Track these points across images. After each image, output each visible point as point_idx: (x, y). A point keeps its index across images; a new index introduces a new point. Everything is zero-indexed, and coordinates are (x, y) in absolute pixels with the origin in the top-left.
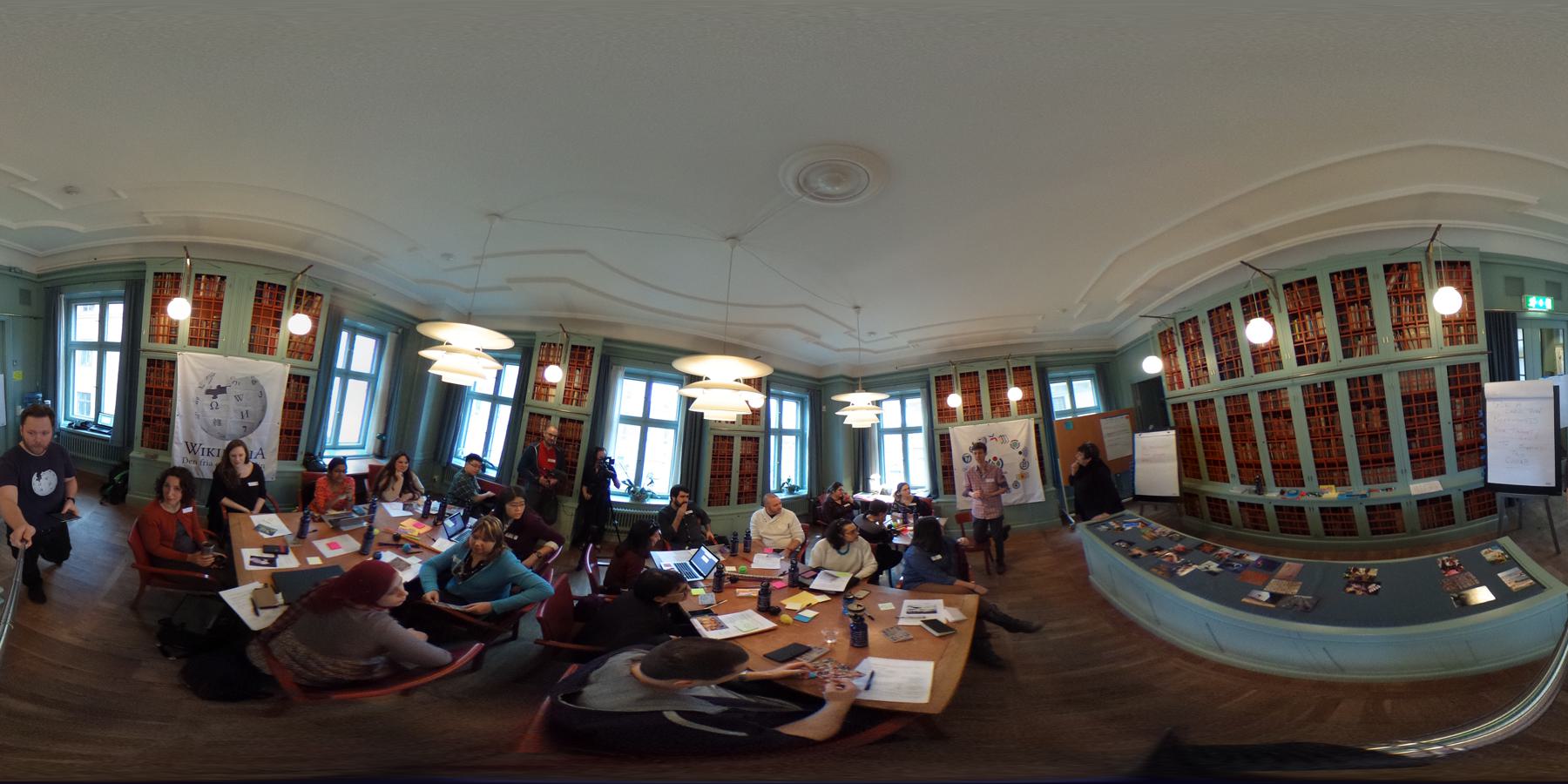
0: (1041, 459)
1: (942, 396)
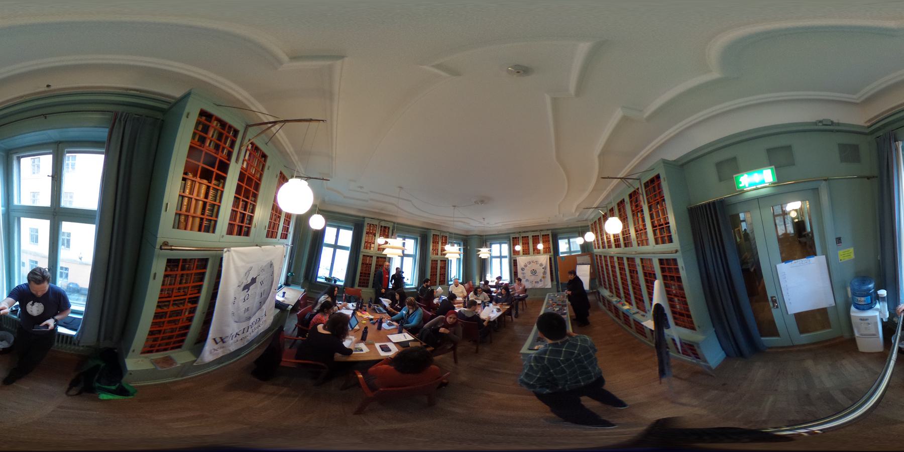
0: (551, 271)
1: (514, 245)
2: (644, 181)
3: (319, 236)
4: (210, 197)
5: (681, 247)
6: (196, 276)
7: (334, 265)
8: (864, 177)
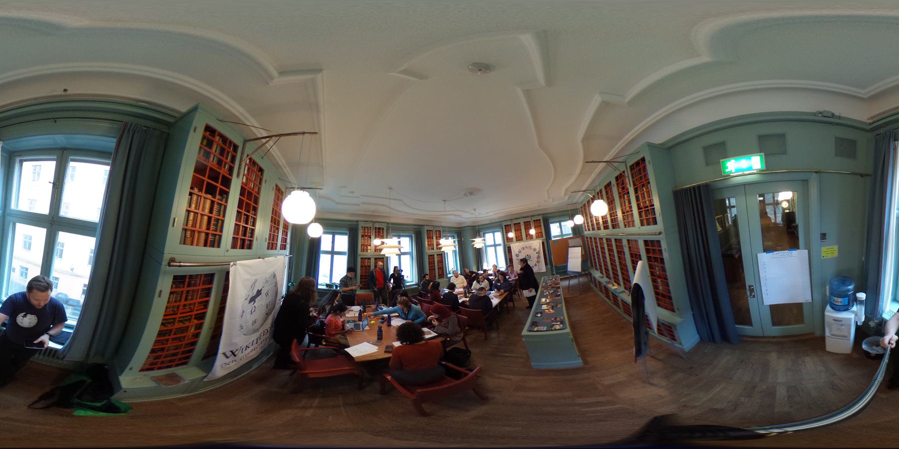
1: (507, 232)
2: (629, 164)
3: (315, 244)
5: (665, 229)
6: (203, 291)
7: (332, 270)
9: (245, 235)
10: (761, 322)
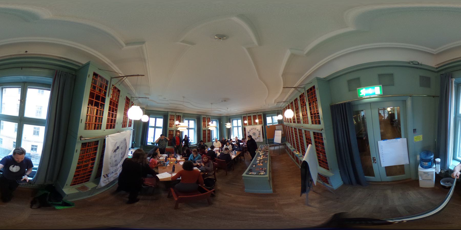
1: (244, 120)
2: (307, 89)
4: (98, 114)
6: (95, 148)
7: (154, 136)
8: (431, 96)
9: (112, 122)
10: (379, 174)
